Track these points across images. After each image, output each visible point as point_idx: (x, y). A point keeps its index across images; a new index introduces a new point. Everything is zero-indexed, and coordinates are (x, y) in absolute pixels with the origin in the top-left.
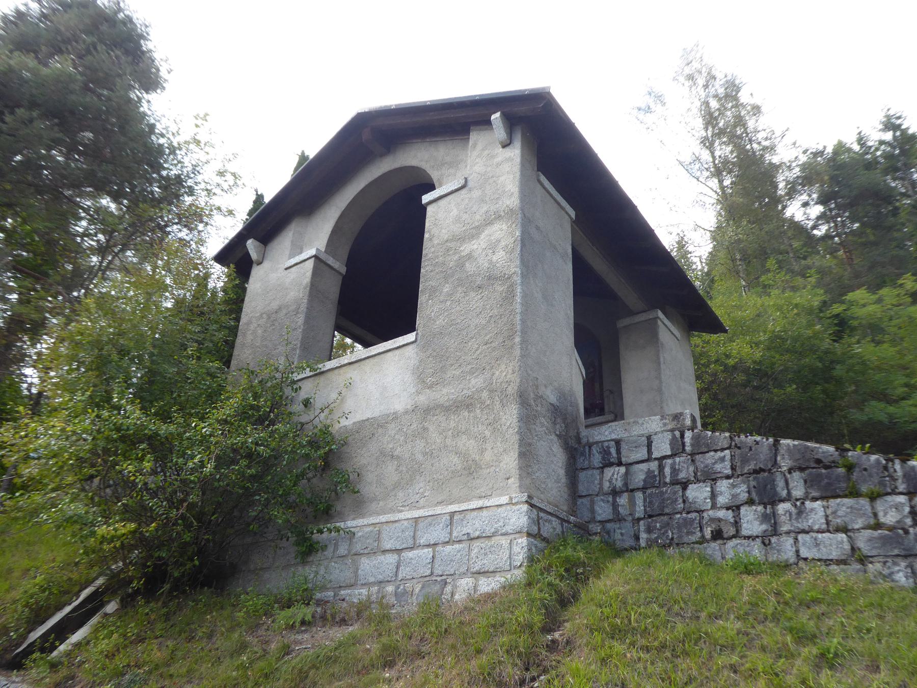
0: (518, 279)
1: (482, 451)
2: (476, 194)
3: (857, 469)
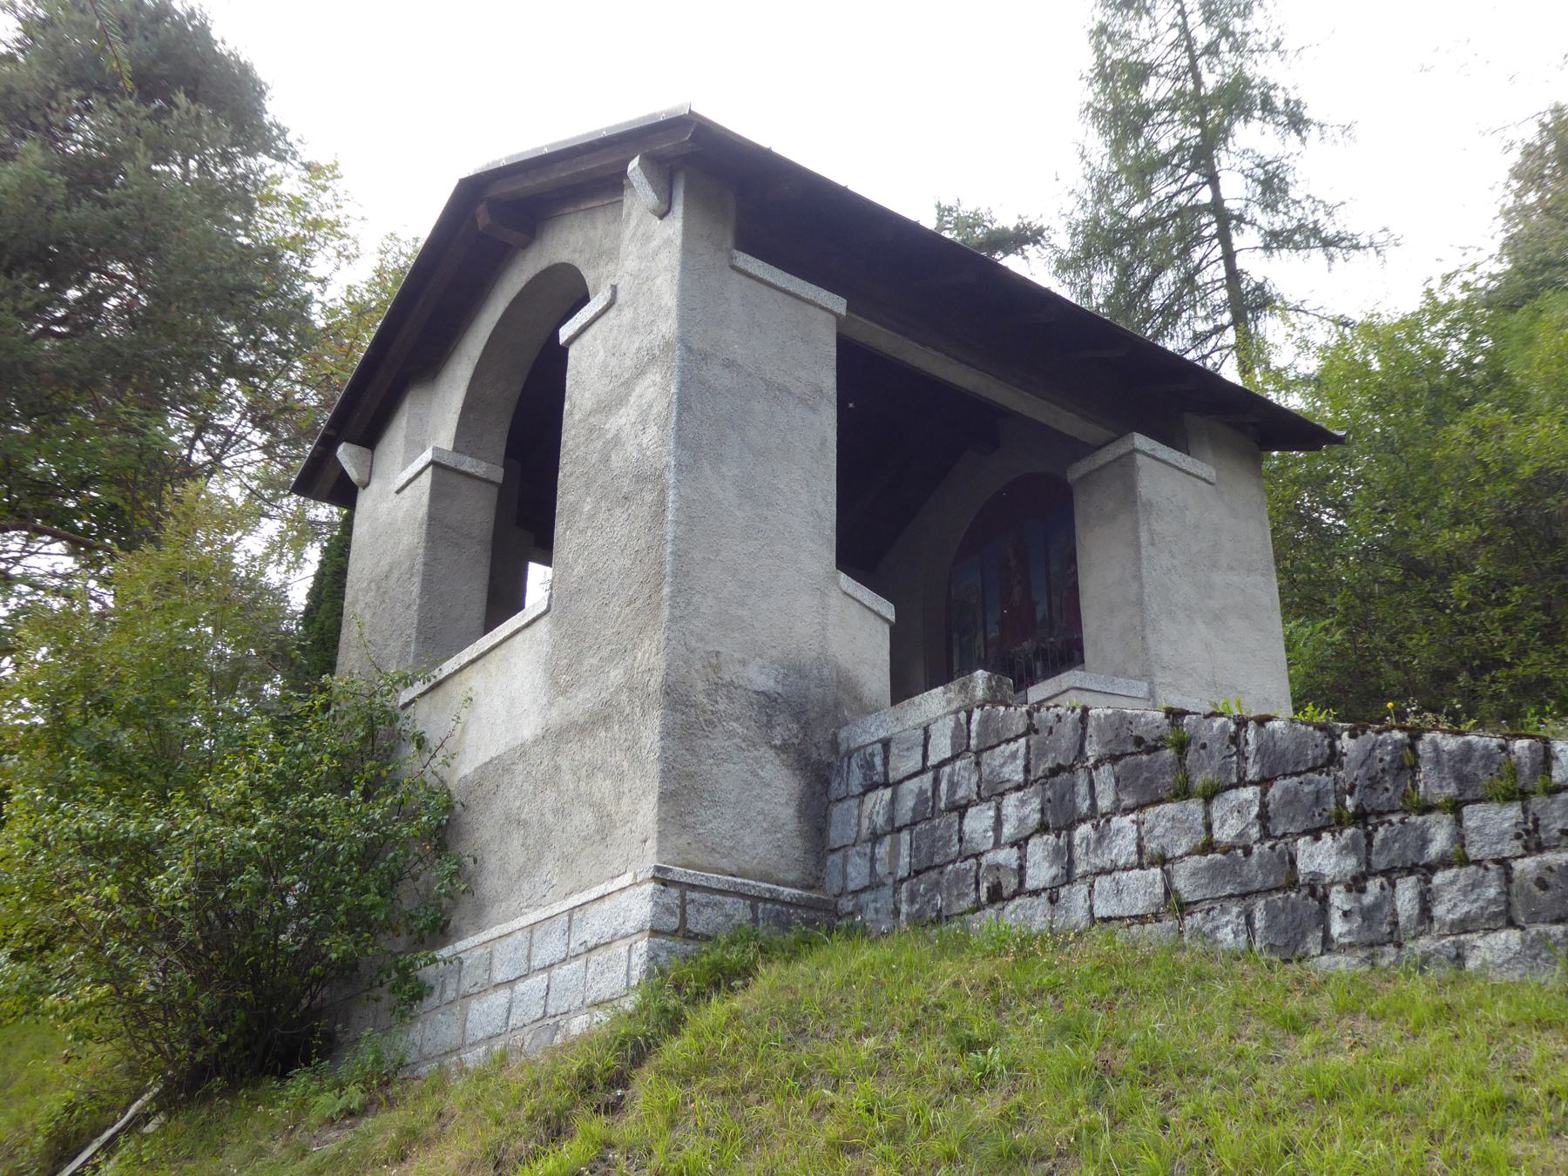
0: (670, 477)
1: (619, 797)
2: (628, 314)
3: (1192, 748)
